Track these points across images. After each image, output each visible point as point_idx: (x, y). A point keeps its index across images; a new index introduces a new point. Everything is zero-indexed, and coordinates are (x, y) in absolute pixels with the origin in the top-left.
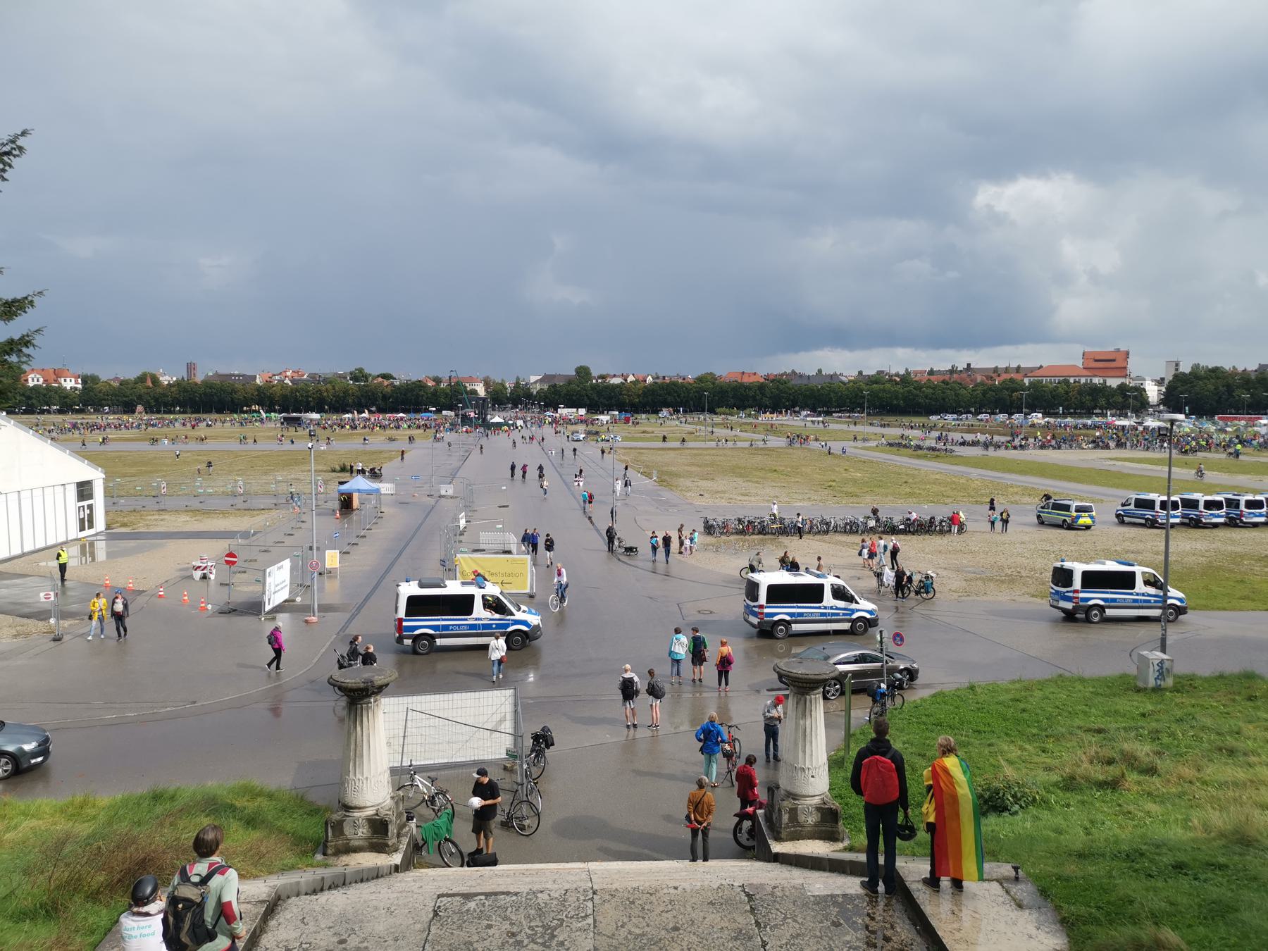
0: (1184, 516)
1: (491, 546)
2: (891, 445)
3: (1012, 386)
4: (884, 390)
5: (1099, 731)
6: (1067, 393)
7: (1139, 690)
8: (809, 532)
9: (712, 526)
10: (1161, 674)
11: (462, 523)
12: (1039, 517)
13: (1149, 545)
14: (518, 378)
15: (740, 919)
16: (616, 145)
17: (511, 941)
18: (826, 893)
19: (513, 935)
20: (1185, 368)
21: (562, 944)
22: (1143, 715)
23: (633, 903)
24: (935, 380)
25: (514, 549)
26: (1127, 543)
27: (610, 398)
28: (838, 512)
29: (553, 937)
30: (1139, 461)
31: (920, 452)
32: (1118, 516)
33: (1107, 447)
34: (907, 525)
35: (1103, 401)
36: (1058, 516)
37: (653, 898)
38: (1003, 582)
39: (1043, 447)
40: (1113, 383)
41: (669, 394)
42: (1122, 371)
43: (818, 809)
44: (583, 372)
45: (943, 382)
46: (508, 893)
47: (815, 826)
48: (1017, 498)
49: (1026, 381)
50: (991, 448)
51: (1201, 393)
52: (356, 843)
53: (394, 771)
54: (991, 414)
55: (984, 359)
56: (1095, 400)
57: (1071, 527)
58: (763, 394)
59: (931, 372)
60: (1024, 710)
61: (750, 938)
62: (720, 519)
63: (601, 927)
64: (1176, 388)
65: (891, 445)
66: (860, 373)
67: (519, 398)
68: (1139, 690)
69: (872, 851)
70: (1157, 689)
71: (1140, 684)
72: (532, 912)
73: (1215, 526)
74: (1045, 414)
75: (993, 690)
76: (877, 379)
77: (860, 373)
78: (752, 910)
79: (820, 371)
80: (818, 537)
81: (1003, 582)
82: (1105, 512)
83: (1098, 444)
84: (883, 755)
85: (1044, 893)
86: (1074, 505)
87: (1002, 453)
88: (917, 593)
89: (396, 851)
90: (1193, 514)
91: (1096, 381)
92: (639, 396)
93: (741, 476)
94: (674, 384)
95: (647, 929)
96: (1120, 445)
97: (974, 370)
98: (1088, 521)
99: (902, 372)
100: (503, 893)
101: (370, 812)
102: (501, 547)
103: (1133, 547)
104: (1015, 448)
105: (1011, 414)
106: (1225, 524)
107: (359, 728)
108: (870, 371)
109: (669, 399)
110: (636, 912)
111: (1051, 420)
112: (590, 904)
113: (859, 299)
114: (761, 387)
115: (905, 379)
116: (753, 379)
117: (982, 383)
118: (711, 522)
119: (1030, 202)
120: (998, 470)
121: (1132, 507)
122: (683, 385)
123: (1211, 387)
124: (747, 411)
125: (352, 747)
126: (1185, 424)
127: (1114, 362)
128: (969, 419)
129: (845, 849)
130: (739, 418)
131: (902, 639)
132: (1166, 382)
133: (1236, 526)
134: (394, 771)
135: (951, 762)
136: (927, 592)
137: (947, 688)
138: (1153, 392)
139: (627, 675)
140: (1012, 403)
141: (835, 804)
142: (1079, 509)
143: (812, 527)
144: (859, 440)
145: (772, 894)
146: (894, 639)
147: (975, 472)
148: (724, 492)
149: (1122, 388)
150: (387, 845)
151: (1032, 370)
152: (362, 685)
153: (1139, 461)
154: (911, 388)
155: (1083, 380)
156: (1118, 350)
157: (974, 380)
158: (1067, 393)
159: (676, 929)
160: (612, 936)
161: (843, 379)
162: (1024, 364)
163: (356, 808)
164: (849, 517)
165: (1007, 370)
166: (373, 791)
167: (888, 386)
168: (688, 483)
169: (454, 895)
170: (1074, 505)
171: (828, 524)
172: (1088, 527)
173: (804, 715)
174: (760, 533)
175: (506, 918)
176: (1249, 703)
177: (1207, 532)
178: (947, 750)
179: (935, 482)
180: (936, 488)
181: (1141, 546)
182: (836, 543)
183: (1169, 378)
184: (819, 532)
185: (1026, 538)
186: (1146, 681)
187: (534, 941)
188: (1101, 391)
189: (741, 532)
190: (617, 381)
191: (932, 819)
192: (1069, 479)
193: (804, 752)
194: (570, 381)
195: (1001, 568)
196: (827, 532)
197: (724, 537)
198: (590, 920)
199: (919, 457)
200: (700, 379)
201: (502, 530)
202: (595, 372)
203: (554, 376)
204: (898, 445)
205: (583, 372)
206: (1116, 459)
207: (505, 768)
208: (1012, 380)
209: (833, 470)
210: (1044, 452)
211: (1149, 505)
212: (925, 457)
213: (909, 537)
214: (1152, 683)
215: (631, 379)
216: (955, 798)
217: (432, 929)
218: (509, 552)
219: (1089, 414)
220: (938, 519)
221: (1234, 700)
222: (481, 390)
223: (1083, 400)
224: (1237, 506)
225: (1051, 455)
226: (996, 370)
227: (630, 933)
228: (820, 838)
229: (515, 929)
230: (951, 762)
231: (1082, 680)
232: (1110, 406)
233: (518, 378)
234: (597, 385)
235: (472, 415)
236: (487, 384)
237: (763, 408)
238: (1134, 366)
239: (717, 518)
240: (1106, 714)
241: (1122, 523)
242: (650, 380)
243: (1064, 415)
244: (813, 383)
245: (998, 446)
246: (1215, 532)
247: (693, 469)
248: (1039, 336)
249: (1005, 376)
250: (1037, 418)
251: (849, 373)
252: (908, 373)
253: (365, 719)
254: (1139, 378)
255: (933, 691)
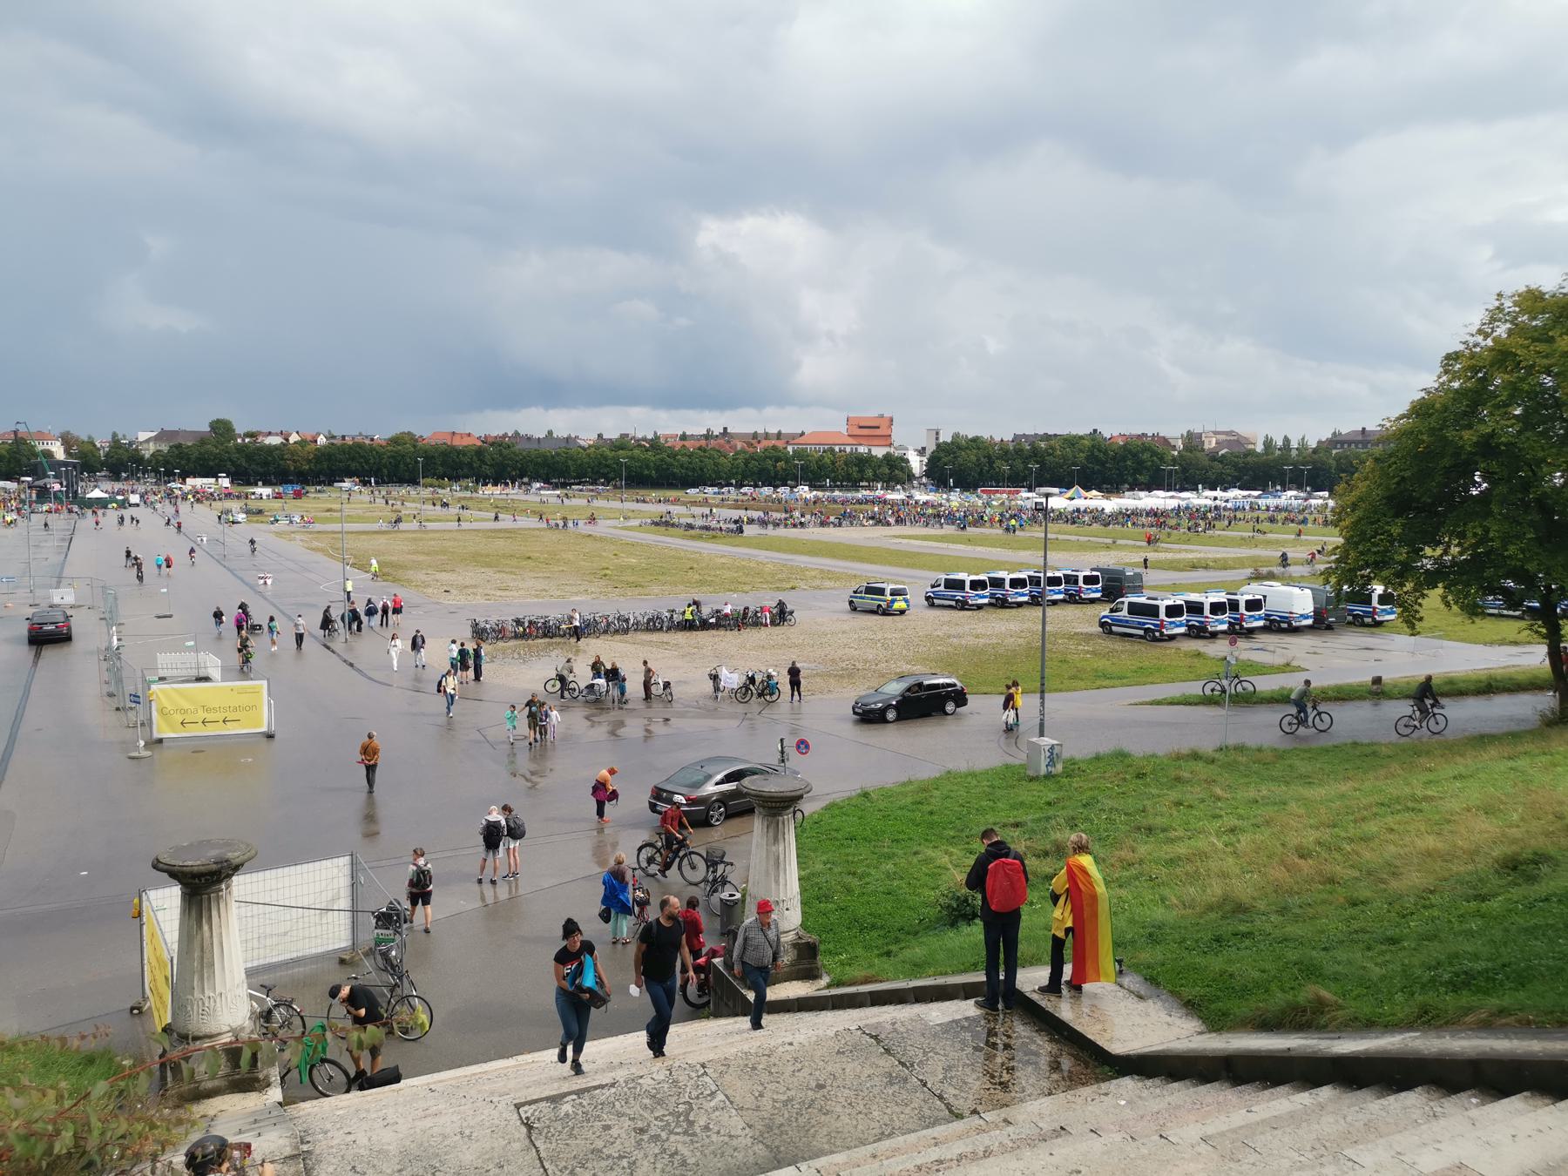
0: (992, 596)
1: (175, 673)
2: (656, 524)
3: (775, 455)
4: (632, 458)
5: (1017, 825)
6: (833, 463)
7: (1032, 779)
8: (605, 632)
9: (484, 630)
10: (1052, 760)
11: (115, 642)
12: (851, 603)
13: (967, 628)
14: (114, 435)
15: (882, 1063)
16: (218, 120)
17: (646, 1137)
18: (947, 1019)
19: (642, 1131)
20: (946, 437)
21: (707, 1128)
22: (1049, 804)
23: (754, 1068)
24: (691, 445)
25: (215, 673)
26: (945, 628)
27: (266, 464)
28: (637, 607)
29: (691, 1123)
30: (925, 538)
31: (692, 532)
32: (928, 598)
33: (888, 524)
34: (718, 618)
35: (869, 473)
36: (873, 602)
37: (772, 1060)
38: (842, 676)
39: (823, 524)
40: (879, 452)
41: (353, 459)
42: (886, 439)
43: (795, 945)
44: (222, 428)
45: (700, 448)
46: (601, 1087)
47: (792, 965)
48: (818, 582)
49: (790, 449)
50: (770, 527)
51: (961, 465)
52: (209, 1085)
53: (250, 973)
54: (756, 486)
55: (743, 422)
56: (861, 471)
57: (886, 612)
58: (483, 462)
59: (684, 437)
60: (931, 813)
61: (905, 1080)
62: (493, 619)
63: (738, 1100)
64: (939, 459)
65: (656, 524)
66: (600, 436)
67: (122, 463)
68: (1032, 779)
69: (991, 970)
70: (1049, 776)
71: (1031, 773)
72: (646, 1101)
73: (1020, 605)
74: (813, 487)
75: (887, 794)
76: (622, 444)
77: (600, 436)
78: (888, 1051)
79: (550, 433)
80: (618, 637)
81: (842, 676)
82: (916, 597)
83: (879, 521)
84: (1007, 855)
85: (1152, 981)
86: (889, 588)
87: (782, 532)
88: (760, 695)
89: (269, 1085)
90: (999, 593)
91: (862, 450)
92: (309, 461)
93: (489, 565)
94: (360, 446)
95: (790, 1093)
96: (899, 521)
97: (732, 436)
98: (903, 605)
99: (650, 436)
100: (596, 1088)
101: (226, 1039)
102: (194, 673)
103: (953, 631)
104: (795, 526)
105: (776, 487)
106: (1063, 601)
107: (206, 927)
108: (612, 434)
109: (354, 465)
110: (765, 1077)
111: (820, 494)
112: (707, 1079)
113: (571, 341)
114: (479, 452)
115: (655, 444)
116: (466, 442)
117: (743, 451)
118: (482, 625)
119: (763, 243)
120: (785, 552)
121: (942, 588)
122: (372, 449)
123: (973, 458)
124: (464, 483)
125: (197, 954)
126: (955, 500)
127: (875, 429)
128: (731, 493)
129: (829, 986)
130: (453, 492)
131: (807, 747)
132: (928, 452)
133: (1076, 602)
134: (250, 973)
135: (1086, 860)
136: (771, 694)
137: (837, 798)
138: (917, 464)
139: (492, 818)
140: (776, 473)
141: (812, 938)
142: (894, 593)
143: (608, 625)
144: (620, 517)
145: (895, 1030)
146: (798, 747)
147: (763, 555)
148: (475, 586)
149: (888, 457)
150: (257, 1080)
151: (794, 436)
152: (214, 867)
153: (925, 538)
154: (664, 455)
155: (848, 449)
156: (882, 416)
157: (733, 448)
158: (833, 463)
159: (820, 1087)
160: (758, 1109)
161: (582, 443)
162: (786, 430)
163: (196, 1038)
164: (651, 612)
165: (767, 436)
166: (230, 1010)
167: (637, 452)
168: (421, 576)
169: (541, 1100)
170: (889, 588)
171: (627, 621)
172: (902, 612)
173: (776, 840)
174: (545, 636)
175: (620, 1115)
176: (1140, 782)
177: (1014, 611)
178: (1081, 848)
179: (723, 566)
180: (728, 574)
181: (960, 630)
182: (643, 643)
183: (931, 448)
184: (617, 631)
185: (846, 627)
186: (1038, 770)
187: (671, 1132)
188: (863, 462)
189: (523, 636)
190: (275, 441)
191: (1069, 924)
192: (861, 560)
193: (777, 882)
194: (202, 440)
195: (833, 661)
196: (626, 631)
197: (500, 644)
198: (720, 1097)
199: (693, 538)
200: (395, 441)
201: (196, 650)
202: (240, 429)
203: (174, 434)
204: (664, 523)
205: (222, 428)
206: (910, 537)
207: (342, 962)
208: (774, 448)
209: (600, 556)
210: (826, 530)
211: (959, 585)
212: (700, 537)
213: (722, 632)
214: (1043, 770)
215: (294, 438)
216: (1094, 898)
217: (538, 1144)
218: (207, 679)
219: (855, 486)
220: (752, 609)
221: (1125, 780)
222: (59, 453)
223: (846, 472)
224: (1076, 582)
225: (832, 534)
226: (755, 435)
227: (775, 1101)
228: (797, 979)
229: (640, 1124)
230: (1086, 860)
231: (973, 775)
232: (876, 478)
233: (114, 435)
234: (245, 446)
235: (57, 487)
236: (67, 441)
237: (482, 479)
238: (897, 438)
239: (489, 619)
240: (1013, 807)
241: (932, 605)
242: (322, 440)
243: (832, 489)
244: (546, 448)
245: (776, 525)
246: (981, 613)
247: (421, 558)
248: (783, 399)
249: (765, 443)
250: (804, 491)
251: (587, 437)
252: (657, 437)
253: (214, 913)
254: (901, 447)
255: (823, 804)
